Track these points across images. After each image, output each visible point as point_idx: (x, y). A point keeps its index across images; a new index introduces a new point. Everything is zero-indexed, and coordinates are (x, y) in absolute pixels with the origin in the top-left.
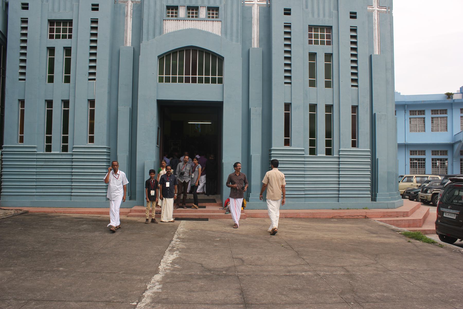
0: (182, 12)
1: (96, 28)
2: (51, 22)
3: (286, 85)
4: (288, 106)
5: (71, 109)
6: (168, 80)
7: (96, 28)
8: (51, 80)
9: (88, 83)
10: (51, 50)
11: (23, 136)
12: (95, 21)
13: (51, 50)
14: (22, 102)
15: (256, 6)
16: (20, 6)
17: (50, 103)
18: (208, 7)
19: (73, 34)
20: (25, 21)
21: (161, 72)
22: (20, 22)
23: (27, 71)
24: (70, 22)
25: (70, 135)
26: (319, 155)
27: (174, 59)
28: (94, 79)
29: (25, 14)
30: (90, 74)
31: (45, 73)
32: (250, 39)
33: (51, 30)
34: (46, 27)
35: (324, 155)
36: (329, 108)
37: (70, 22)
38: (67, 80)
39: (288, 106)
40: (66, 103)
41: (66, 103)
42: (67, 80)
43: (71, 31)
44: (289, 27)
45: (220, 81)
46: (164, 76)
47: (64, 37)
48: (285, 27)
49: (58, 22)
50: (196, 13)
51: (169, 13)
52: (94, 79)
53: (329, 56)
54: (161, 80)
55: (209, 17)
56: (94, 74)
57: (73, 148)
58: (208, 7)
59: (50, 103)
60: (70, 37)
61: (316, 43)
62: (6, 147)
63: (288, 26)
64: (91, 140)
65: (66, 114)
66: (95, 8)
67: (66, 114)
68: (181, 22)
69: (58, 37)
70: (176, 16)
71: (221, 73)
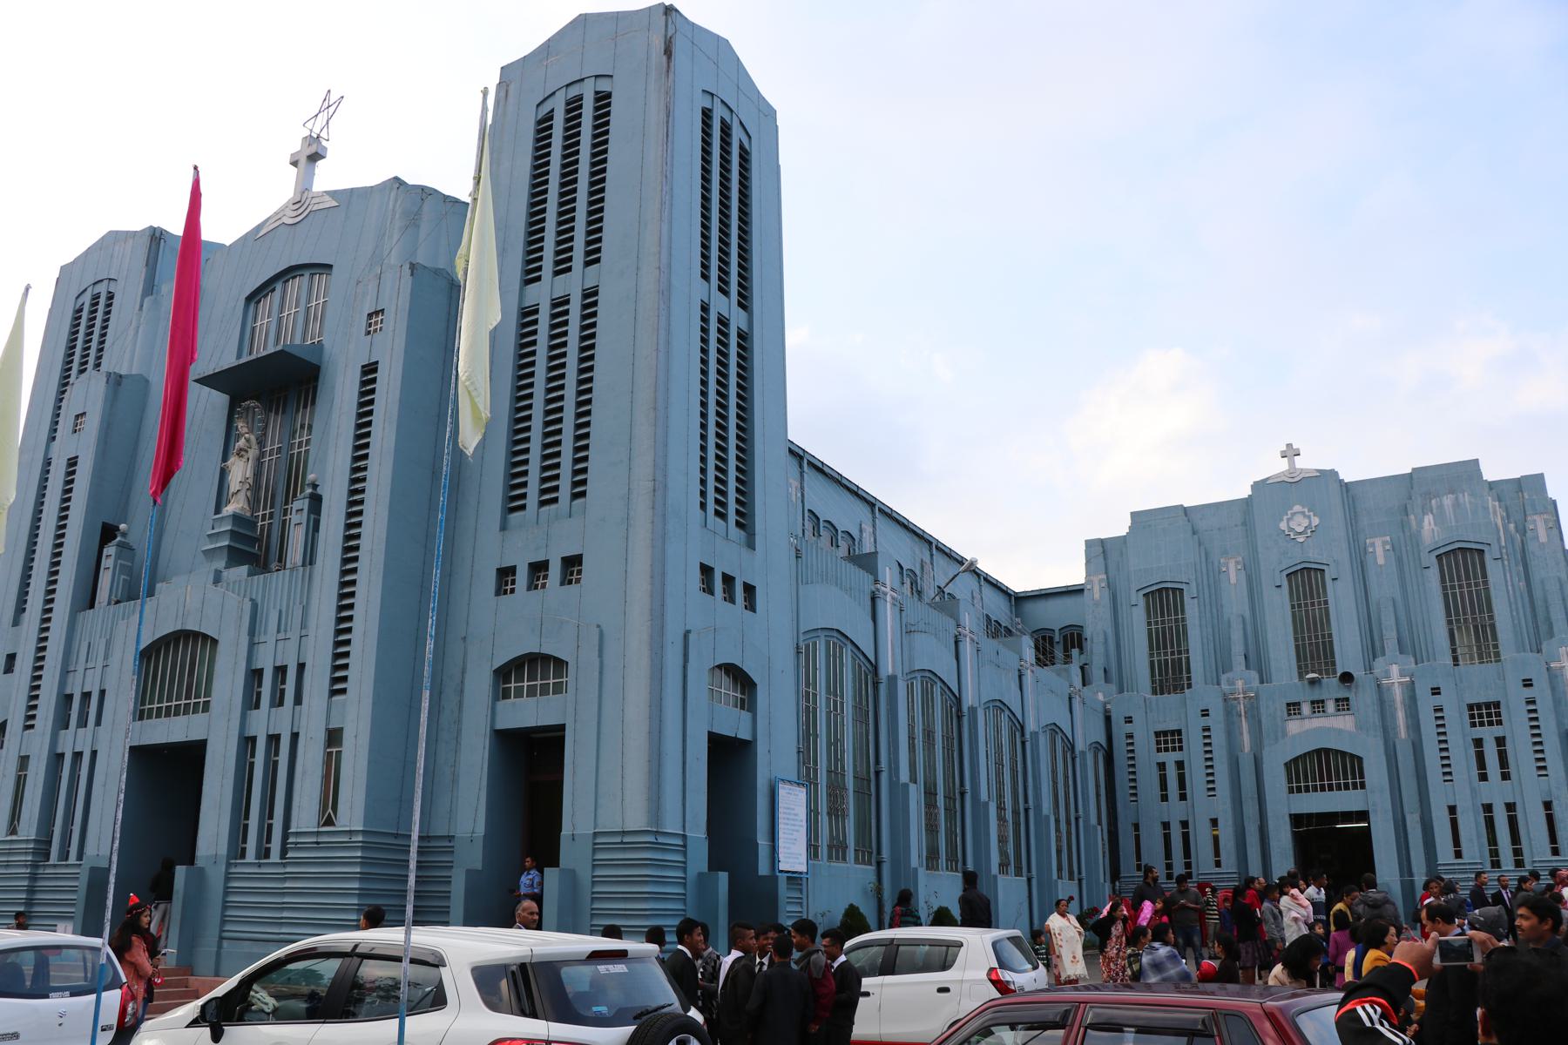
0: (1306, 709)
1: (1209, 737)
2: (1157, 734)
3: (1446, 783)
4: (1452, 809)
5: (1187, 771)
6: (1299, 790)
7: (1209, 737)
8: (1165, 798)
9: (1186, 515)
10: (1162, 766)
11: (1139, 835)
12: (1207, 729)
13: (1162, 766)
14: (1137, 827)
15: (1396, 685)
16: (1123, 721)
17: (1166, 825)
18: (1336, 699)
19: (1184, 744)
20: (1130, 736)
21: (1290, 781)
22: (1125, 738)
23: (1139, 791)
24: (1179, 732)
25: (1193, 860)
26: (1504, 868)
27: (1303, 576)
28: (1215, 795)
29: (1128, 728)
30: (1209, 789)
31: (1157, 792)
32: (1395, 727)
33: (1158, 743)
34: (1153, 739)
35: (1513, 868)
36: (1510, 807)
37: (1179, 732)
38: (1183, 797)
39: (1452, 809)
40: (1185, 824)
41: (1185, 824)
42: (1183, 797)
43: (1180, 741)
44: (1441, 710)
45: (1363, 786)
46: (1295, 785)
47: (1174, 749)
48: (1436, 711)
49: (1165, 733)
50: (1323, 707)
51: (1290, 710)
52: (1215, 795)
53: (1500, 741)
54: (1291, 791)
55: (1339, 710)
56: (1213, 789)
57: (1199, 874)
58: (1336, 699)
59: (1166, 825)
60: (1181, 749)
61: (1482, 724)
62: (1124, 877)
63: (1439, 709)
64: (1218, 864)
65: (1186, 837)
66: (1205, 713)
67: (1186, 837)
68: (1307, 721)
69: (1166, 750)
70: (1300, 714)
71: (1362, 776)
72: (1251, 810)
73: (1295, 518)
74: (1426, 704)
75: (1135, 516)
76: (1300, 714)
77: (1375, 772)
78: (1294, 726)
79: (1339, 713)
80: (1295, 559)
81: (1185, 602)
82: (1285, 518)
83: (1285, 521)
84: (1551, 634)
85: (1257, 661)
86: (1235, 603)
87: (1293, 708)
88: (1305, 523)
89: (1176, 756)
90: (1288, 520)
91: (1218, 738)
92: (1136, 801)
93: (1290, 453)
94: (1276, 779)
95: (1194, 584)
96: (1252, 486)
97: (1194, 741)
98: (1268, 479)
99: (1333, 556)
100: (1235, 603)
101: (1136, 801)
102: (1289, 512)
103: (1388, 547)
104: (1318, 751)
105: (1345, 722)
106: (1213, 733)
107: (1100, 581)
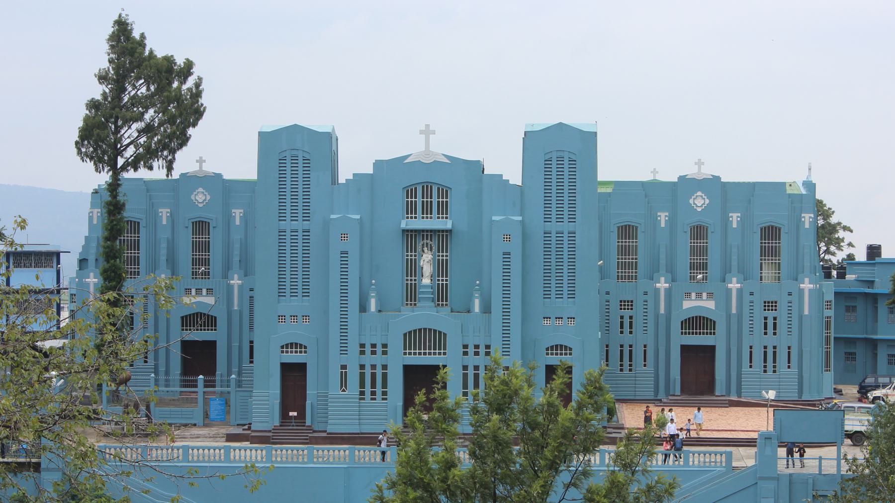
6: (686, 333)
11: (622, 350)
45: (714, 333)
54: (682, 333)
72: (734, 341)
73: (697, 198)
74: (747, 298)
75: (815, 184)
76: (201, 294)
77: (222, 323)
78: (186, 300)
79: (132, 295)
80: (694, 221)
81: (140, 229)
82: (693, 197)
83: (693, 199)
84: (803, 272)
85: (172, 263)
86: (164, 235)
87: (188, 291)
88: (204, 198)
89: (630, 312)
90: (694, 199)
91: (651, 305)
92: (608, 333)
93: (201, 161)
94: (676, 327)
95: (144, 220)
96: (678, 178)
97: (782, 307)
98: (686, 175)
99: (213, 217)
100: (164, 235)
101: (608, 333)
102: (706, 197)
103: (168, 215)
104: (197, 313)
105: (210, 300)
106: (648, 303)
107: (98, 212)
